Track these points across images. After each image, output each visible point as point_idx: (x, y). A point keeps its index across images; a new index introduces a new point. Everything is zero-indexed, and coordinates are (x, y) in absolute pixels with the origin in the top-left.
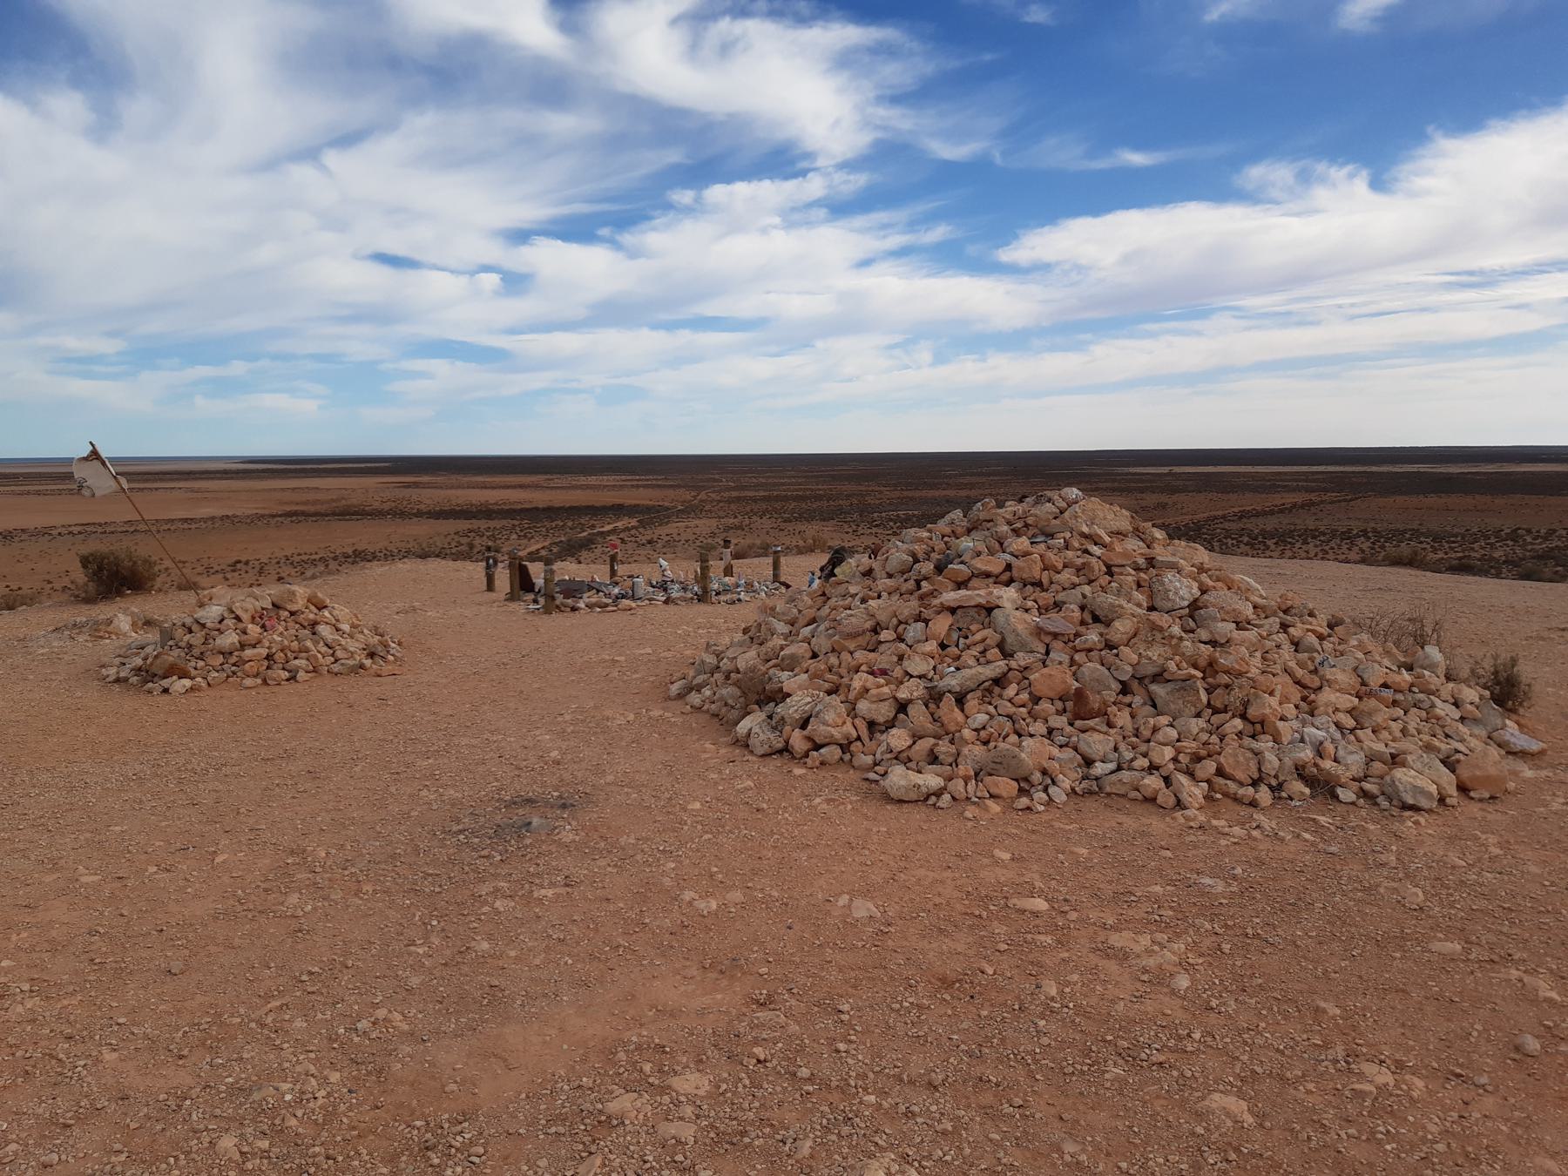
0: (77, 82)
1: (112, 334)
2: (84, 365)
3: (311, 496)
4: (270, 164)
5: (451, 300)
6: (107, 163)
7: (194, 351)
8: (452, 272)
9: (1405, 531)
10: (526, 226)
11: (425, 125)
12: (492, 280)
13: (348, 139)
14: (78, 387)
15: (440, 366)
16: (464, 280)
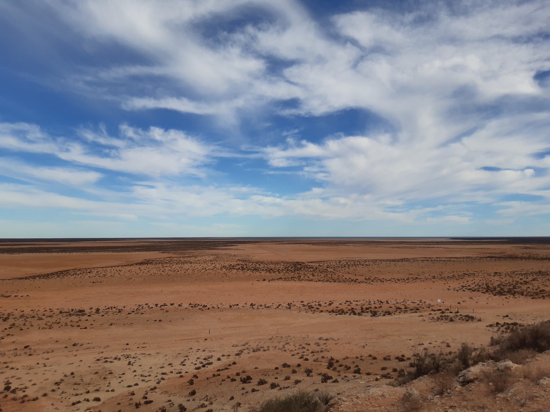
0: (386, 131)
1: (401, 199)
2: (393, 209)
3: (489, 251)
4: (445, 144)
5: (513, 180)
6: (395, 151)
7: (426, 203)
8: (514, 170)
10: (543, 151)
11: (494, 125)
12: (530, 172)
13: (468, 133)
14: (392, 215)
15: (516, 204)
16: (519, 173)
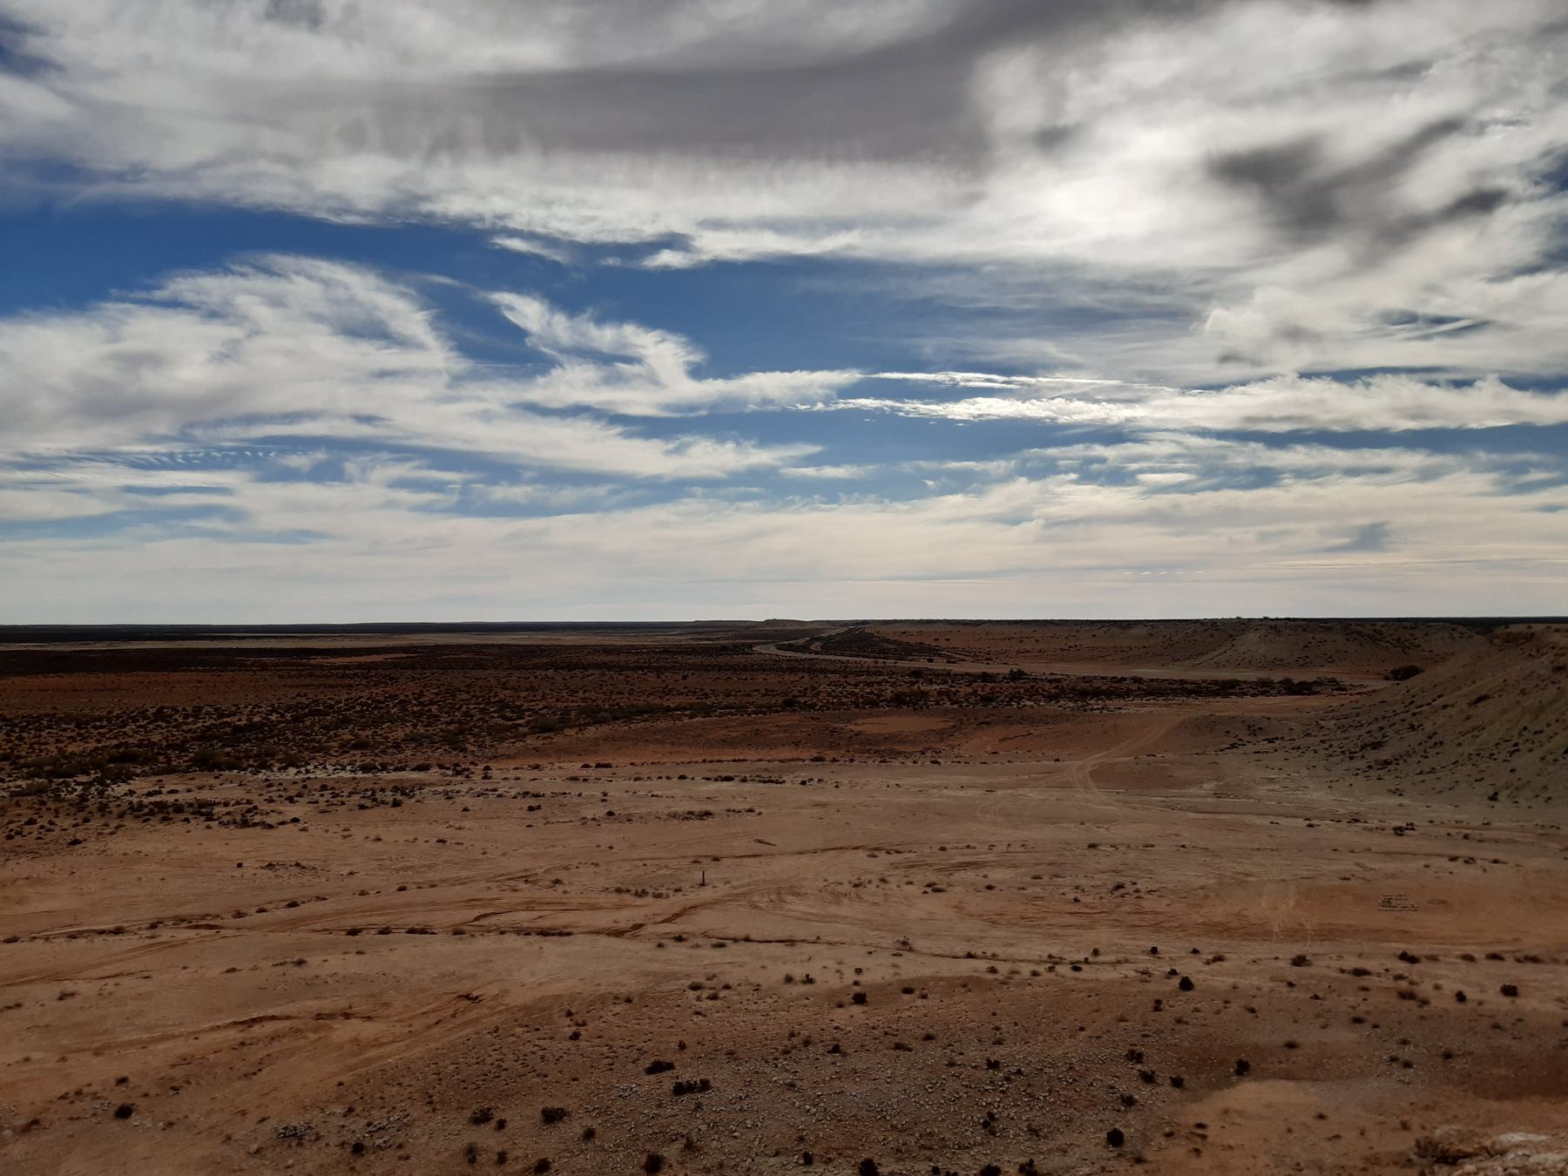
9: (39, 718)
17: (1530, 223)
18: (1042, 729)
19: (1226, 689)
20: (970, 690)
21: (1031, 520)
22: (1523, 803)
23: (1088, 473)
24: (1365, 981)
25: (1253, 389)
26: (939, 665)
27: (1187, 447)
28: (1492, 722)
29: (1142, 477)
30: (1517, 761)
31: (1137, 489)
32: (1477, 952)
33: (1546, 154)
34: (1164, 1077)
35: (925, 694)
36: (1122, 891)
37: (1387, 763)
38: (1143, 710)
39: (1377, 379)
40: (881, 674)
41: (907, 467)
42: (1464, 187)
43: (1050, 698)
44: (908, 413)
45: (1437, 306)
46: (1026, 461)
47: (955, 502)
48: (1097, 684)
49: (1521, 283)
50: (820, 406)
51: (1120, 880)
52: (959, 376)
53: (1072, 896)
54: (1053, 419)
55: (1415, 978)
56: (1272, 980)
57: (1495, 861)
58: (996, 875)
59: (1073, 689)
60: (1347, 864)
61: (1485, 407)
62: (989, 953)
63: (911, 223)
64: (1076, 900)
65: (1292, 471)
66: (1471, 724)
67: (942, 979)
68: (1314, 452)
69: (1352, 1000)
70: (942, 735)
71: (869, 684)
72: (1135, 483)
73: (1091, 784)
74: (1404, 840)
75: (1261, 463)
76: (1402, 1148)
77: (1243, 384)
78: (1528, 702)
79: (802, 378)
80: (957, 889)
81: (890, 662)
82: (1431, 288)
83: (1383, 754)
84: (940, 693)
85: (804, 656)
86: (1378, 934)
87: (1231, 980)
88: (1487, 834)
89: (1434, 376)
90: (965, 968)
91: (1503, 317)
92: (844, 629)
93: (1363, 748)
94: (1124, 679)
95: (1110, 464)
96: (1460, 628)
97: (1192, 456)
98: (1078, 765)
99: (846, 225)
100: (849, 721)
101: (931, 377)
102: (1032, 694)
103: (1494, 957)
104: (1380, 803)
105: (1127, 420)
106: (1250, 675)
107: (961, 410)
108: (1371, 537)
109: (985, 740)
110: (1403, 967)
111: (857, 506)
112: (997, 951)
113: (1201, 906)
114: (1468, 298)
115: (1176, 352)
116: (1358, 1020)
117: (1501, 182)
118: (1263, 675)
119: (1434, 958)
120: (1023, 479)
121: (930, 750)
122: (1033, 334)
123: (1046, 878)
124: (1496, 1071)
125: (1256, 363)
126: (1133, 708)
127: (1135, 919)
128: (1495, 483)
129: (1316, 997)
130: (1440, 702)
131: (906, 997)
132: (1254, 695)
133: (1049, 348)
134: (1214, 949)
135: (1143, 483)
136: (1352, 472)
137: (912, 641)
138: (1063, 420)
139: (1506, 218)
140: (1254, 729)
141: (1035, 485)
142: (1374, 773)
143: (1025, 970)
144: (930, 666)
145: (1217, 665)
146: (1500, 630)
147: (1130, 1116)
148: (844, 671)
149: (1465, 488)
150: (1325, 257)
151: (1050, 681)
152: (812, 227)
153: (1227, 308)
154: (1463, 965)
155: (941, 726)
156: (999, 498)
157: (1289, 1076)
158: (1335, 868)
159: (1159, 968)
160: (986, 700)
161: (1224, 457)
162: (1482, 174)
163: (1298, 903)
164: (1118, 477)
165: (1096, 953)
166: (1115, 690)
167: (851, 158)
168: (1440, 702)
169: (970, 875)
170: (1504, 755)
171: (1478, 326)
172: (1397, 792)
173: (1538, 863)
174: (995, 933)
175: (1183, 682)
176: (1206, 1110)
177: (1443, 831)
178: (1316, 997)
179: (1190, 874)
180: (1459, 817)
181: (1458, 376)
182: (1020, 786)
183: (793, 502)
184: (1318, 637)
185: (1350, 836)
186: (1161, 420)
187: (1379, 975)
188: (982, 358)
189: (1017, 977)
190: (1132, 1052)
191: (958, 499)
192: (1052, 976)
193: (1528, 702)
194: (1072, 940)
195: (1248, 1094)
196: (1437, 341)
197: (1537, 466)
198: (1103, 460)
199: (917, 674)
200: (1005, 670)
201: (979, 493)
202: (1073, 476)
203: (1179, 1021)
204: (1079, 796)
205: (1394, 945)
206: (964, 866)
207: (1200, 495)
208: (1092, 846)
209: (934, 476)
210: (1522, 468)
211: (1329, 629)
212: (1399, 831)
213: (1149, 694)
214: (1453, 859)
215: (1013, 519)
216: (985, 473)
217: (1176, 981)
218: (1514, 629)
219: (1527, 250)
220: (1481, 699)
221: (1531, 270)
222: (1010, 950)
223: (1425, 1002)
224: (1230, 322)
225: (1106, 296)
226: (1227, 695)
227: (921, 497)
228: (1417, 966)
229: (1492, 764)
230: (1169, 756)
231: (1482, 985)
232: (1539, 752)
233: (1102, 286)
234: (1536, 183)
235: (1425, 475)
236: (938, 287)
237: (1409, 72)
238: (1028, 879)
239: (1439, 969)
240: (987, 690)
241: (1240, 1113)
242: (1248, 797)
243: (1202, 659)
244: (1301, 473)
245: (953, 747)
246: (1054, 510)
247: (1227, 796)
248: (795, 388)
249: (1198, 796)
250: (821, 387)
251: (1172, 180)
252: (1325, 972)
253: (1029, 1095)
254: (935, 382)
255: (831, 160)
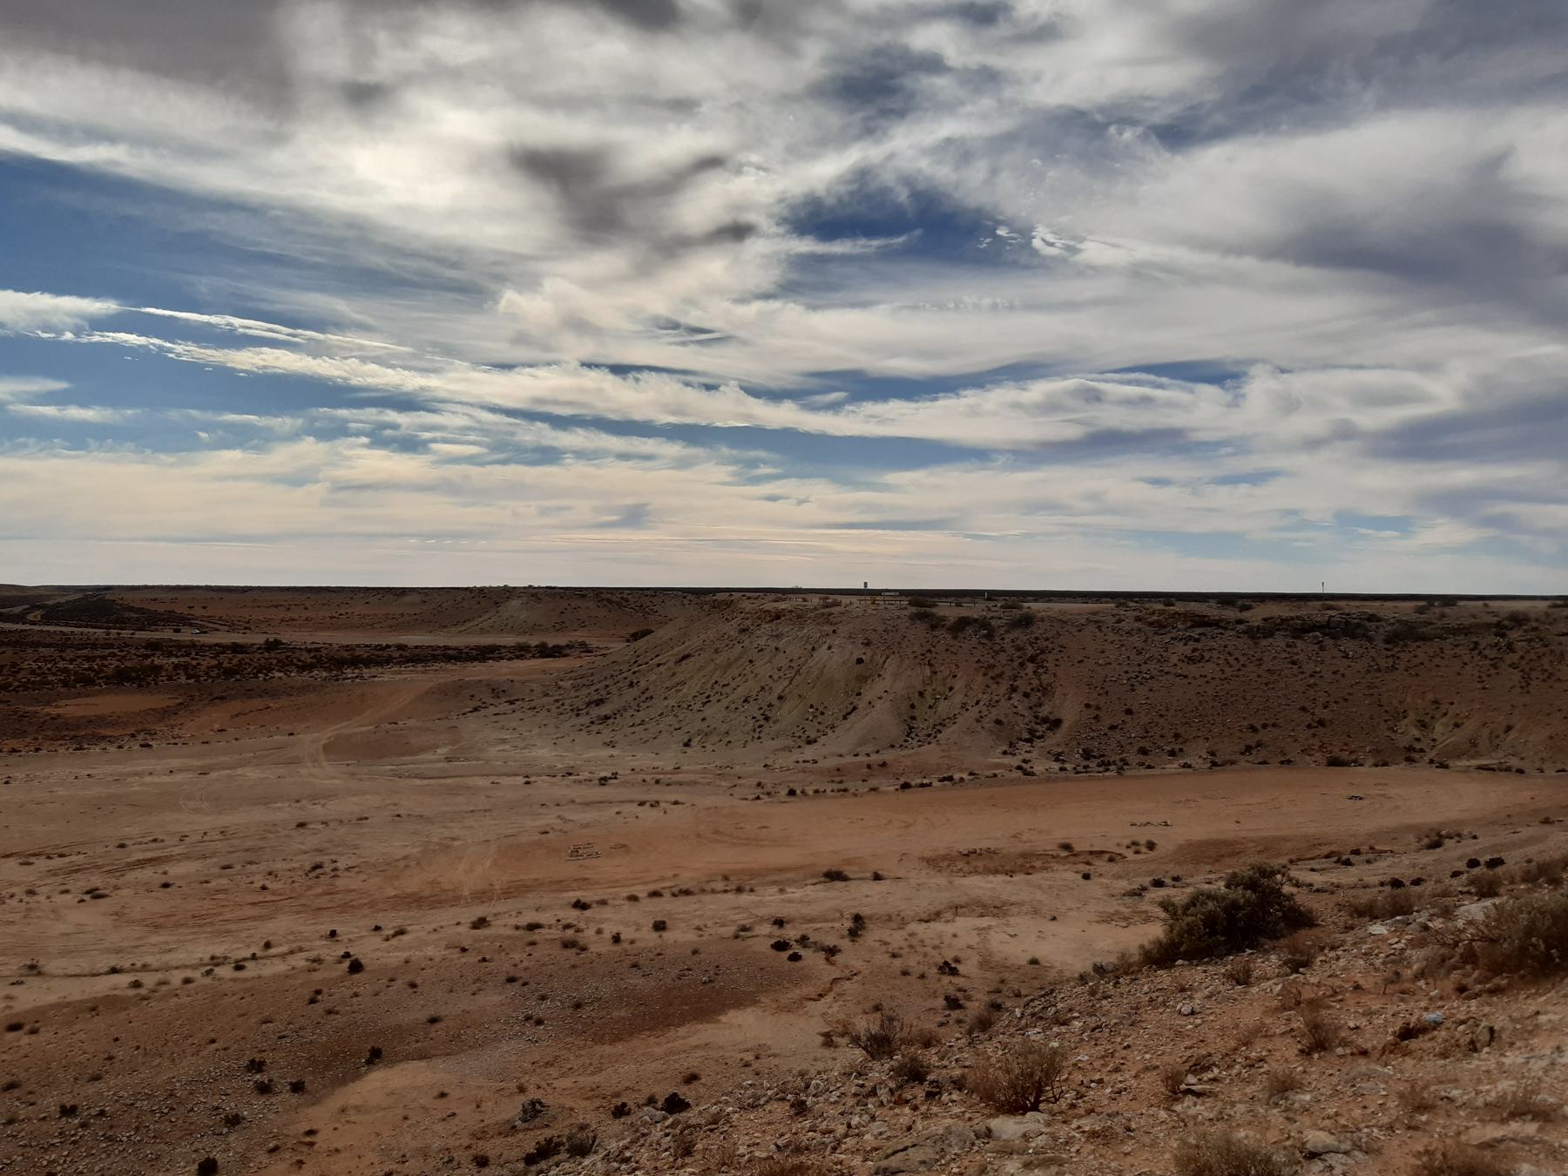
17: (764, 256)
18: (284, 701)
19: (485, 654)
20: (215, 662)
21: (317, 481)
22: (709, 747)
23: (380, 438)
24: (536, 936)
25: (541, 372)
26: (187, 635)
27: (479, 421)
28: (691, 678)
29: (433, 446)
30: (708, 711)
31: (430, 457)
32: (641, 891)
33: (780, 201)
34: (282, 1085)
35: (156, 669)
36: (319, 871)
37: (607, 718)
38: (398, 677)
39: (645, 375)
40: (111, 646)
41: (174, 415)
42: (726, 219)
43: (305, 667)
44: (179, 355)
45: (694, 317)
46: (315, 419)
47: (232, 457)
48: (358, 652)
49: (756, 307)
50: (69, 336)
51: (319, 859)
52: (237, 321)
53: (258, 885)
54: (345, 379)
55: (582, 925)
56: (447, 947)
57: (676, 803)
58: (176, 870)
59: (332, 658)
60: (549, 819)
61: (727, 409)
62: (139, 965)
63: (194, 151)
64: (264, 888)
65: (573, 452)
66: (676, 679)
67: (68, 1005)
68: (592, 436)
69: (517, 957)
70: (164, 714)
71: (88, 659)
72: (427, 451)
73: (322, 757)
74: (606, 789)
75: (545, 442)
76: (505, 1116)
77: (531, 366)
78: (720, 659)
79: (42, 301)
80: (125, 892)
81: (126, 633)
82: (690, 301)
83: (605, 710)
84: (176, 667)
85: (20, 627)
86: (560, 885)
87: (406, 955)
88: (680, 777)
89: (689, 378)
90: (103, 986)
91: (742, 334)
92: (80, 595)
93: (588, 704)
94: (388, 646)
95: (402, 432)
96: (690, 597)
97: (484, 430)
98: (311, 738)
99: (112, 138)
100: (48, 703)
101: (205, 318)
102: (284, 666)
103: (655, 894)
104: (594, 755)
105: (422, 389)
106: (510, 640)
107: (244, 360)
108: (634, 516)
109: (216, 716)
110: (572, 915)
111: (110, 455)
112: (149, 959)
113: (397, 877)
114: (715, 314)
115: (467, 326)
116: (511, 980)
117: (752, 217)
118: (522, 640)
119: (603, 903)
120: (311, 439)
121: (142, 732)
122: (323, 289)
123: (238, 867)
124: (615, 1014)
125: (547, 348)
126: (387, 676)
127: (323, 902)
128: (734, 474)
129: (484, 960)
130: (656, 661)
131: (11, 1035)
132: (510, 659)
133: (341, 306)
134: (397, 923)
135: (435, 453)
136: (624, 456)
137: (161, 609)
138: (355, 381)
139: (755, 247)
140: (497, 692)
141: (323, 446)
142: (594, 728)
143: (176, 978)
144: (175, 637)
145: (482, 631)
146: (709, 598)
147: (232, 1138)
148: (64, 644)
149: (711, 476)
150: (607, 261)
151: (309, 651)
152: (63, 131)
153: (520, 293)
154: (627, 905)
155: (164, 704)
156: (280, 458)
157: (422, 1056)
158: (538, 823)
159: (334, 951)
160: (229, 673)
161: (513, 434)
162: (739, 207)
163: (495, 863)
164: (410, 445)
165: (268, 945)
166: (379, 658)
167: (110, 61)
168: (656, 661)
169: (147, 874)
170: (699, 705)
171: (724, 340)
172: (611, 744)
173: (709, 801)
174: (154, 939)
175: (446, 648)
176: (319, 1115)
177: (641, 777)
178: (484, 960)
179: (399, 844)
180: (656, 764)
181: (709, 381)
182: (241, 766)
183: (25, 446)
184: (573, 604)
185: (563, 790)
186: (456, 392)
187: (550, 927)
188: (264, 306)
189: (164, 988)
190: (253, 1062)
191: (236, 454)
192: (208, 980)
193: (720, 659)
194: (244, 934)
195: (377, 1083)
196: (692, 348)
197: (765, 462)
198: (395, 427)
199: (154, 646)
200: (260, 639)
201: (259, 449)
202: (365, 440)
203: (329, 1012)
204: (303, 771)
205: (571, 894)
206: (142, 863)
207: (489, 468)
208: (301, 825)
209: (209, 427)
210: (754, 463)
211: (583, 596)
212: (603, 781)
213: (409, 661)
214: (642, 804)
215: (296, 480)
216: (269, 430)
217: (347, 963)
218: (719, 597)
219: (766, 278)
220: (684, 658)
221: (767, 296)
222: (167, 957)
223: (584, 949)
224: (527, 306)
225: (401, 262)
226: (484, 660)
227: (190, 449)
228: (587, 913)
229: (689, 714)
230: (411, 723)
231: (633, 923)
232: (725, 702)
233: (399, 252)
234: (778, 224)
235: (682, 464)
236: (215, 223)
237: (682, 106)
238: (216, 870)
239: (606, 913)
240: (235, 661)
241: (358, 1108)
242: (478, 759)
243: (468, 625)
244: (580, 454)
245: (173, 727)
246: (342, 473)
247: (458, 759)
248: (34, 313)
249: (431, 762)
250: (69, 314)
251: (477, 162)
252: (502, 931)
253: (110, 1139)
254: (209, 324)
255: (84, 58)
